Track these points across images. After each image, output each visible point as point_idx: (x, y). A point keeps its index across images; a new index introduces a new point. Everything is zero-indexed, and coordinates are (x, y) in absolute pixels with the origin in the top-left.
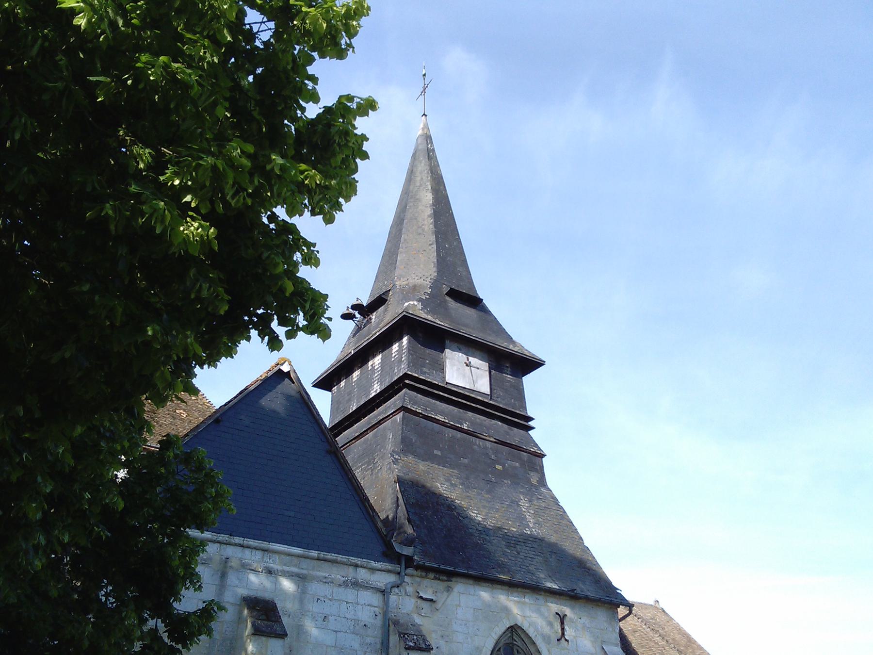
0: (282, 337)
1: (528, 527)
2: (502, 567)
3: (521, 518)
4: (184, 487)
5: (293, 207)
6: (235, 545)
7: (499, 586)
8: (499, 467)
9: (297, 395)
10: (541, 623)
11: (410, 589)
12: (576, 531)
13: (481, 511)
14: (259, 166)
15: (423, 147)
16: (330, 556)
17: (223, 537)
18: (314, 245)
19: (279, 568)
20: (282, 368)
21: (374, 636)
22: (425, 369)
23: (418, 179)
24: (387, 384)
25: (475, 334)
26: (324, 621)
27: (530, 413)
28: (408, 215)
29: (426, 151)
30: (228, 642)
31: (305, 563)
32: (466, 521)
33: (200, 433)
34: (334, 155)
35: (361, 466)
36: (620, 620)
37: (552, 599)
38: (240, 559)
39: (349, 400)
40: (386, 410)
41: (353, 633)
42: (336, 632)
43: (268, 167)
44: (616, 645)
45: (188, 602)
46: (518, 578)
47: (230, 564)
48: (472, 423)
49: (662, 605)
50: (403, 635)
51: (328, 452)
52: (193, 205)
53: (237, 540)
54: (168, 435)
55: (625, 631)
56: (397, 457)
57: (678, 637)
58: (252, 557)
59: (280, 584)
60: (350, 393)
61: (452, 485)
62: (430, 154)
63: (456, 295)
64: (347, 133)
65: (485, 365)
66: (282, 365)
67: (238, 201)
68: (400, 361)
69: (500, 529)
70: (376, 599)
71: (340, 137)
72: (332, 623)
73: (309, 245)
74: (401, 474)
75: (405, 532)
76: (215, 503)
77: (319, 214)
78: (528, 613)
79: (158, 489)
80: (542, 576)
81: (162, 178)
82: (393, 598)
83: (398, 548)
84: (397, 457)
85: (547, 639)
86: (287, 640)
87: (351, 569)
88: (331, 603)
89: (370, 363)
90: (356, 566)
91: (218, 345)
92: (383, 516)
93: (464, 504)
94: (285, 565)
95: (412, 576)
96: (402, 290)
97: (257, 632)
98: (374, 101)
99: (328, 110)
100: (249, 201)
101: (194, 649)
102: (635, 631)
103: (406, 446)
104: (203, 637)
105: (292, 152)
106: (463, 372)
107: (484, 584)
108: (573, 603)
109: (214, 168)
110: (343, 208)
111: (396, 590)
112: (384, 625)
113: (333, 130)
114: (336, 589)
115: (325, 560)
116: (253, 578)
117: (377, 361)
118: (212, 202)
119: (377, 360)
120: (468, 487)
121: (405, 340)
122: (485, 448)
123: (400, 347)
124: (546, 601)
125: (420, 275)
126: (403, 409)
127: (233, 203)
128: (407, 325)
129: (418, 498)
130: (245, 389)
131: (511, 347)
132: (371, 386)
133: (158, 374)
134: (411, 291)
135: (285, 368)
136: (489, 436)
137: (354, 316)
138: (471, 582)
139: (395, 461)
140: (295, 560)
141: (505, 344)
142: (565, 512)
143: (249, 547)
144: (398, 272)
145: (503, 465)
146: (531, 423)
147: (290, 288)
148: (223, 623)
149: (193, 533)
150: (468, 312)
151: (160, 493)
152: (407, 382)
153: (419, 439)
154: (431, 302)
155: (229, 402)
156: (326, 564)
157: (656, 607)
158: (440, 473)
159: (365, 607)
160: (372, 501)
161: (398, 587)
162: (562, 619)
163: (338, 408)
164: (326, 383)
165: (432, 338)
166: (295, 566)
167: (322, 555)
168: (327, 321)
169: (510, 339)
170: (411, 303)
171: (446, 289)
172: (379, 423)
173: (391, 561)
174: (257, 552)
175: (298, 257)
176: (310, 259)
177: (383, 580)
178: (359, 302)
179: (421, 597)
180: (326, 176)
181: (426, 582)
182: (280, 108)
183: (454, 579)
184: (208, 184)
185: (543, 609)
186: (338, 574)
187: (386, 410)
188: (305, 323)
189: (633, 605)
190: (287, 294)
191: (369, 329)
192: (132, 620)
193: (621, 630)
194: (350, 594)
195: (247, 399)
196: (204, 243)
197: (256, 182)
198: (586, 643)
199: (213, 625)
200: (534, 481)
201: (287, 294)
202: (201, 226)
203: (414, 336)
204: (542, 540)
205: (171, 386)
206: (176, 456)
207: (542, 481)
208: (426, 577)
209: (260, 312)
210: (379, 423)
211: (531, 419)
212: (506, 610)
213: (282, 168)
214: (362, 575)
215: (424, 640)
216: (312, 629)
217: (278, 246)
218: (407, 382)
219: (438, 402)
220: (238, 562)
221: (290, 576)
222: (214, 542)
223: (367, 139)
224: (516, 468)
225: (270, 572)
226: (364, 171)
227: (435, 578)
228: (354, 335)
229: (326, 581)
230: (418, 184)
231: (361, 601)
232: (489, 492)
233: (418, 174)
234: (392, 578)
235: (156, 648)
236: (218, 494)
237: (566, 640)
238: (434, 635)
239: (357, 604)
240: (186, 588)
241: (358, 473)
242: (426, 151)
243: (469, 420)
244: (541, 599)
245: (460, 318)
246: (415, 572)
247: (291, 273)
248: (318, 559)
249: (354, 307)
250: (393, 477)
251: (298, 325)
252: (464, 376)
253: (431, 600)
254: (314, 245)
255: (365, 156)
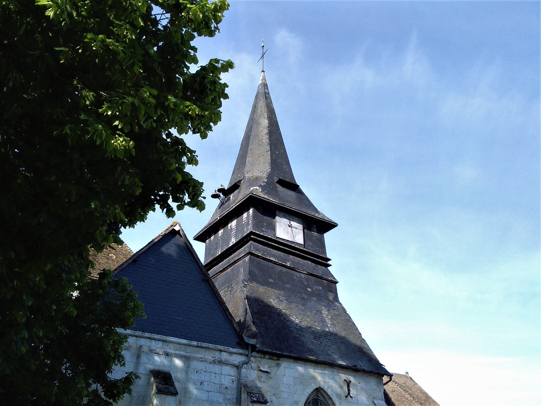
0: (175, 209)
1: (327, 326)
2: (311, 351)
3: (323, 321)
4: (114, 302)
5: (182, 129)
6: (146, 338)
7: (309, 364)
8: (309, 290)
9: (184, 245)
10: (335, 386)
11: (254, 365)
12: (357, 329)
13: (298, 317)
14: (161, 103)
15: (262, 91)
16: (204, 345)
17: (138, 333)
18: (195, 152)
19: (173, 352)
20: (175, 228)
21: (232, 394)
22: (263, 229)
23: (259, 111)
24: (240, 238)
25: (294, 207)
26: (201, 385)
27: (328, 256)
28: (253, 133)
29: (264, 94)
30: (142, 398)
31: (189, 349)
32: (289, 323)
33: (124, 269)
34: (207, 96)
35: (224, 289)
36: (385, 384)
37: (342, 371)
38: (149, 347)
39: (216, 248)
40: (239, 254)
41: (219, 392)
42: (208, 392)
43: (166, 104)
44: (382, 400)
45: (117, 373)
46: (321, 358)
47: (142, 350)
48: (293, 262)
49: (410, 375)
50: (249, 394)
51: (204, 280)
52: (120, 127)
53: (147, 335)
54: (104, 270)
55: (387, 391)
56: (246, 283)
57: (420, 395)
58: (156, 346)
59: (174, 362)
60: (217, 244)
61: (280, 300)
62: (267, 96)
63: (284, 183)
64: (215, 82)
65: (300, 227)
66: (175, 226)
67: (148, 125)
68: (248, 224)
69: (310, 328)
70: (233, 371)
71: (211, 85)
72: (206, 386)
73: (192, 152)
74: (249, 294)
75: (251, 330)
76: (133, 312)
77: (198, 133)
78: (327, 380)
79: (98, 303)
80: (336, 357)
81: (100, 110)
82: (243, 371)
83: (247, 340)
84: (246, 283)
85: (339, 396)
86: (178, 397)
87: (217, 353)
88: (205, 374)
89: (229, 225)
90: (221, 351)
91: (135, 215)
92: (237, 320)
93: (288, 312)
94: (177, 350)
95: (255, 357)
96: (249, 180)
97: (160, 391)
98: (232, 62)
99: (203, 68)
100: (154, 125)
101: (120, 402)
102: (393, 391)
103: (252, 277)
104: (126, 395)
105: (181, 94)
106: (287, 231)
107: (300, 362)
108: (355, 373)
109: (133, 104)
110: (213, 129)
111: (246, 366)
112: (238, 387)
113: (206, 81)
114: (208, 365)
115: (202, 347)
116: (157, 358)
117: (233, 224)
118: (131, 125)
119: (234, 223)
120: (290, 302)
121: (251, 211)
122: (301, 278)
123: (248, 215)
124: (339, 373)
125: (261, 171)
126: (250, 253)
127: (144, 126)
128: (252, 201)
129: (258, 307)
130: (152, 241)
131: (317, 215)
132: (230, 239)
133: (98, 232)
134: (255, 181)
135: (177, 228)
136: (303, 271)
137: (219, 196)
138: (292, 361)
139: (245, 286)
140: (183, 347)
141: (313, 213)
142: (350, 317)
143: (154, 339)
144: (246, 169)
145: (312, 288)
146: (329, 262)
147: (180, 178)
148: (138, 386)
149: (120, 330)
150: (291, 194)
151: (99, 306)
152: (252, 237)
153: (259, 272)
154: (267, 187)
155: (142, 249)
156: (202, 349)
157: (406, 376)
158: (273, 293)
159: (226, 376)
160: (230, 311)
161: (247, 364)
162: (348, 383)
163: (209, 253)
164: (202, 237)
165: (268, 210)
166: (183, 351)
167: (200, 344)
168: (202, 199)
169: (316, 210)
170: (255, 188)
171: (276, 179)
172: (235, 262)
173: (242, 348)
174: (159, 342)
175: (184, 159)
176: (192, 160)
177: (237, 359)
178: (223, 187)
179: (261, 370)
180: (202, 109)
181: (264, 361)
182: (173, 67)
183: (281, 359)
184: (129, 114)
185: (337, 377)
186: (209, 355)
187: (239, 254)
188: (189, 200)
189: (392, 375)
190: (178, 182)
191: (229, 204)
192: (82, 384)
193: (385, 390)
194: (217, 368)
195: (153, 247)
196: (127, 150)
197: (159, 113)
198: (363, 398)
199: (132, 387)
200: (331, 298)
201: (178, 182)
202: (124, 140)
203: (256, 208)
204: (336, 335)
205: (106, 239)
206: (109, 282)
207: (336, 298)
208: (264, 358)
209: (161, 193)
210: (235, 262)
211: (329, 260)
212: (314, 378)
213: (175, 104)
214: (225, 356)
215: (263, 397)
216: (193, 390)
217: (172, 153)
218: (252, 237)
219: (271, 249)
220: (148, 348)
221: (180, 357)
222: (133, 336)
223: (228, 86)
224: (320, 290)
225: (167, 354)
226: (225, 106)
227: (270, 358)
228: (219, 208)
229: (202, 360)
230: (259, 114)
231: (224, 373)
232: (303, 305)
233: (259, 108)
234: (243, 359)
235: (97, 402)
236: (135, 306)
237: (351, 397)
238: (269, 394)
239: (221, 374)
240: (115, 365)
241: (222, 293)
242: (264, 94)
243: (290, 261)
244: (335, 371)
245: (285, 197)
246: (257, 355)
247: (180, 169)
248: (197, 347)
249: (219, 190)
250: (243, 296)
251: (184, 201)
252: (288, 233)
253: (267, 372)
254: (195, 152)
255: (226, 97)
